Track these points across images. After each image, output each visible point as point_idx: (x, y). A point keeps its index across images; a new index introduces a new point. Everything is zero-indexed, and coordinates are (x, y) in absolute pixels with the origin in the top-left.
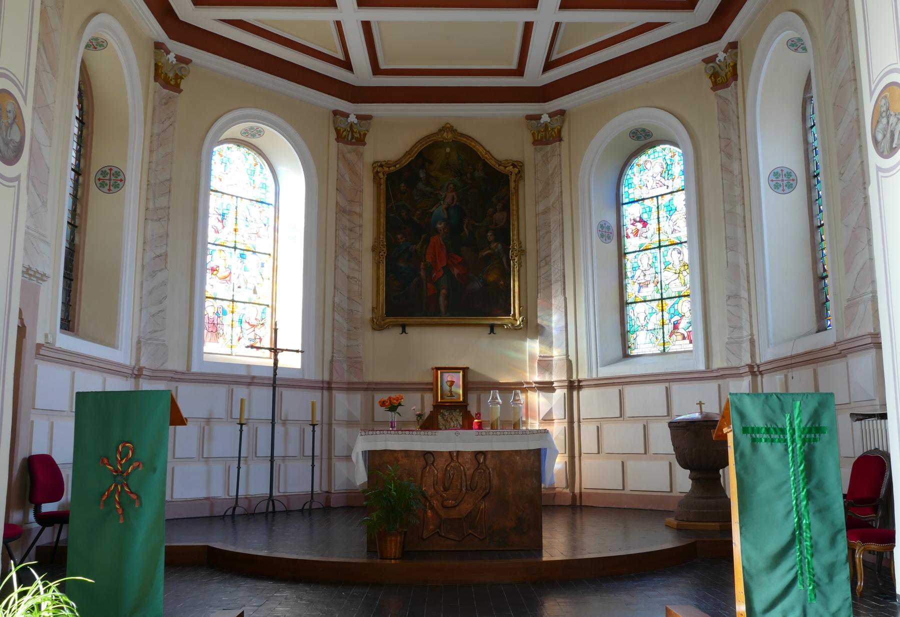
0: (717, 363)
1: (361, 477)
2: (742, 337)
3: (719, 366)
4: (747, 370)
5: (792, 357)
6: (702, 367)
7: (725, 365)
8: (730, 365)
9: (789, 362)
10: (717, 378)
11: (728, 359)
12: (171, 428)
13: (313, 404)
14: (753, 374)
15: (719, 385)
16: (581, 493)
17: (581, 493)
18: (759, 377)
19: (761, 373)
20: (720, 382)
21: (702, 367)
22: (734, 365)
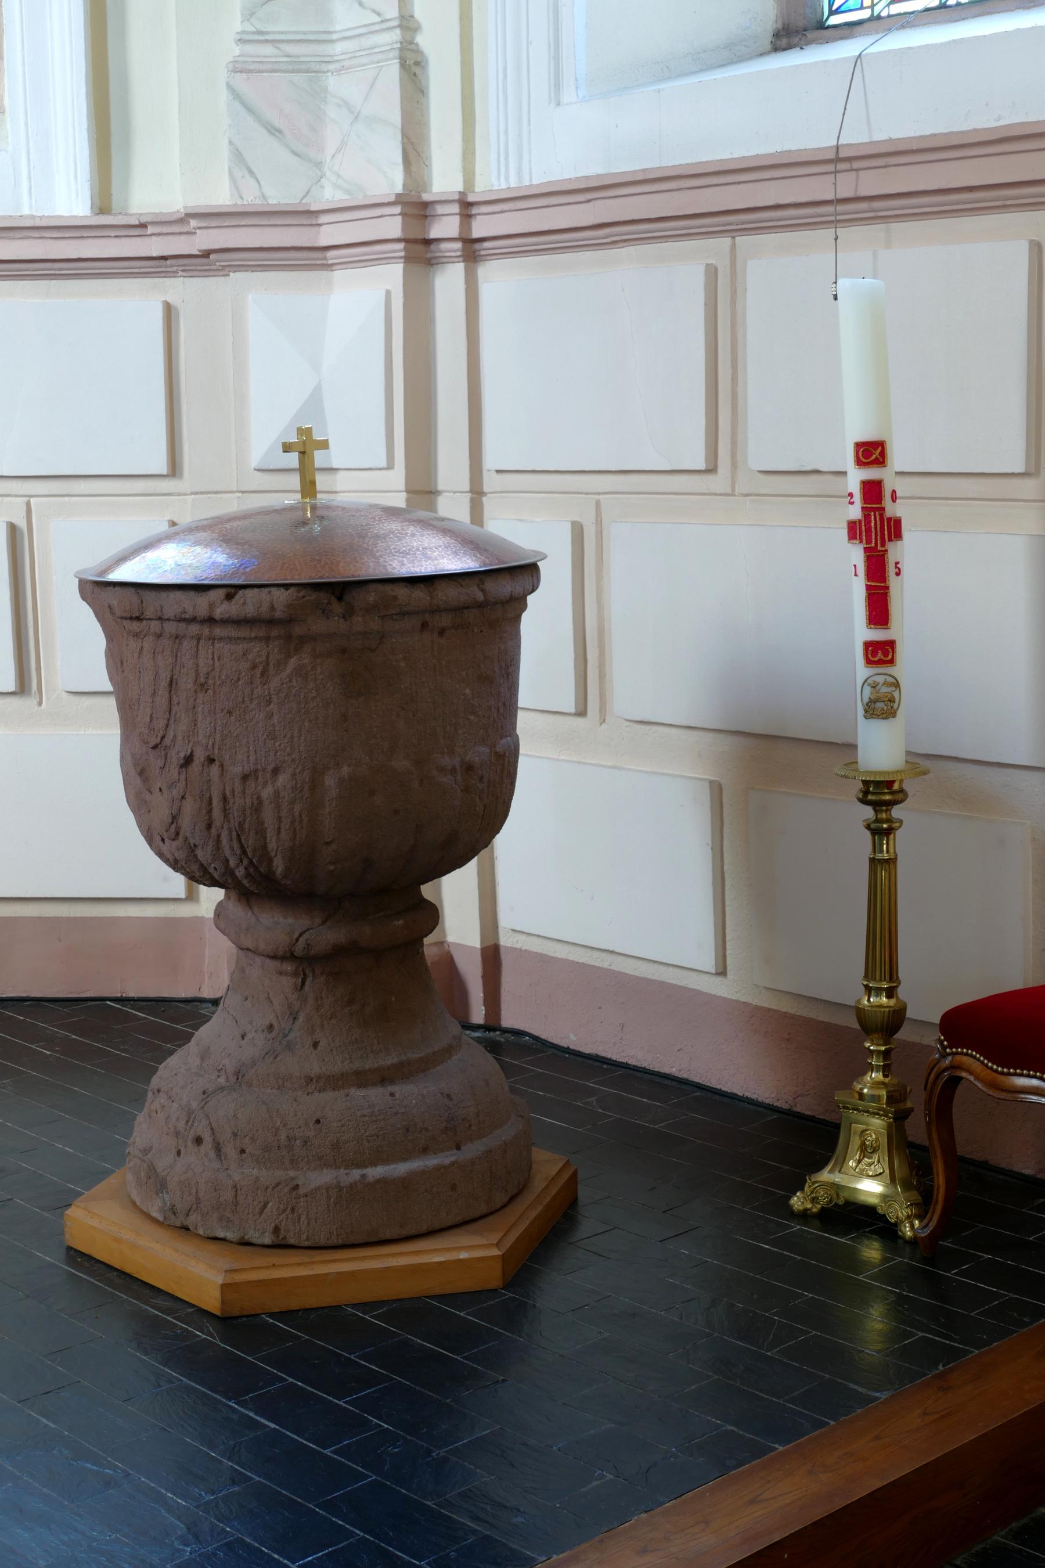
0: (160, 185)
1: (211, 897)
2: (324, 39)
3: (174, 199)
4: (393, 226)
5: (838, 160)
6: (70, 199)
7: (221, 195)
8: (250, 198)
9: (821, 188)
10: (161, 265)
11: (238, 157)
12: (319, 496)
13: (388, 293)
14: (420, 252)
15: (169, 312)
16: (492, 956)
17: (492, 956)
18: (449, 281)
19: (472, 250)
20: (178, 289)
21: (70, 199)
22: (277, 197)
